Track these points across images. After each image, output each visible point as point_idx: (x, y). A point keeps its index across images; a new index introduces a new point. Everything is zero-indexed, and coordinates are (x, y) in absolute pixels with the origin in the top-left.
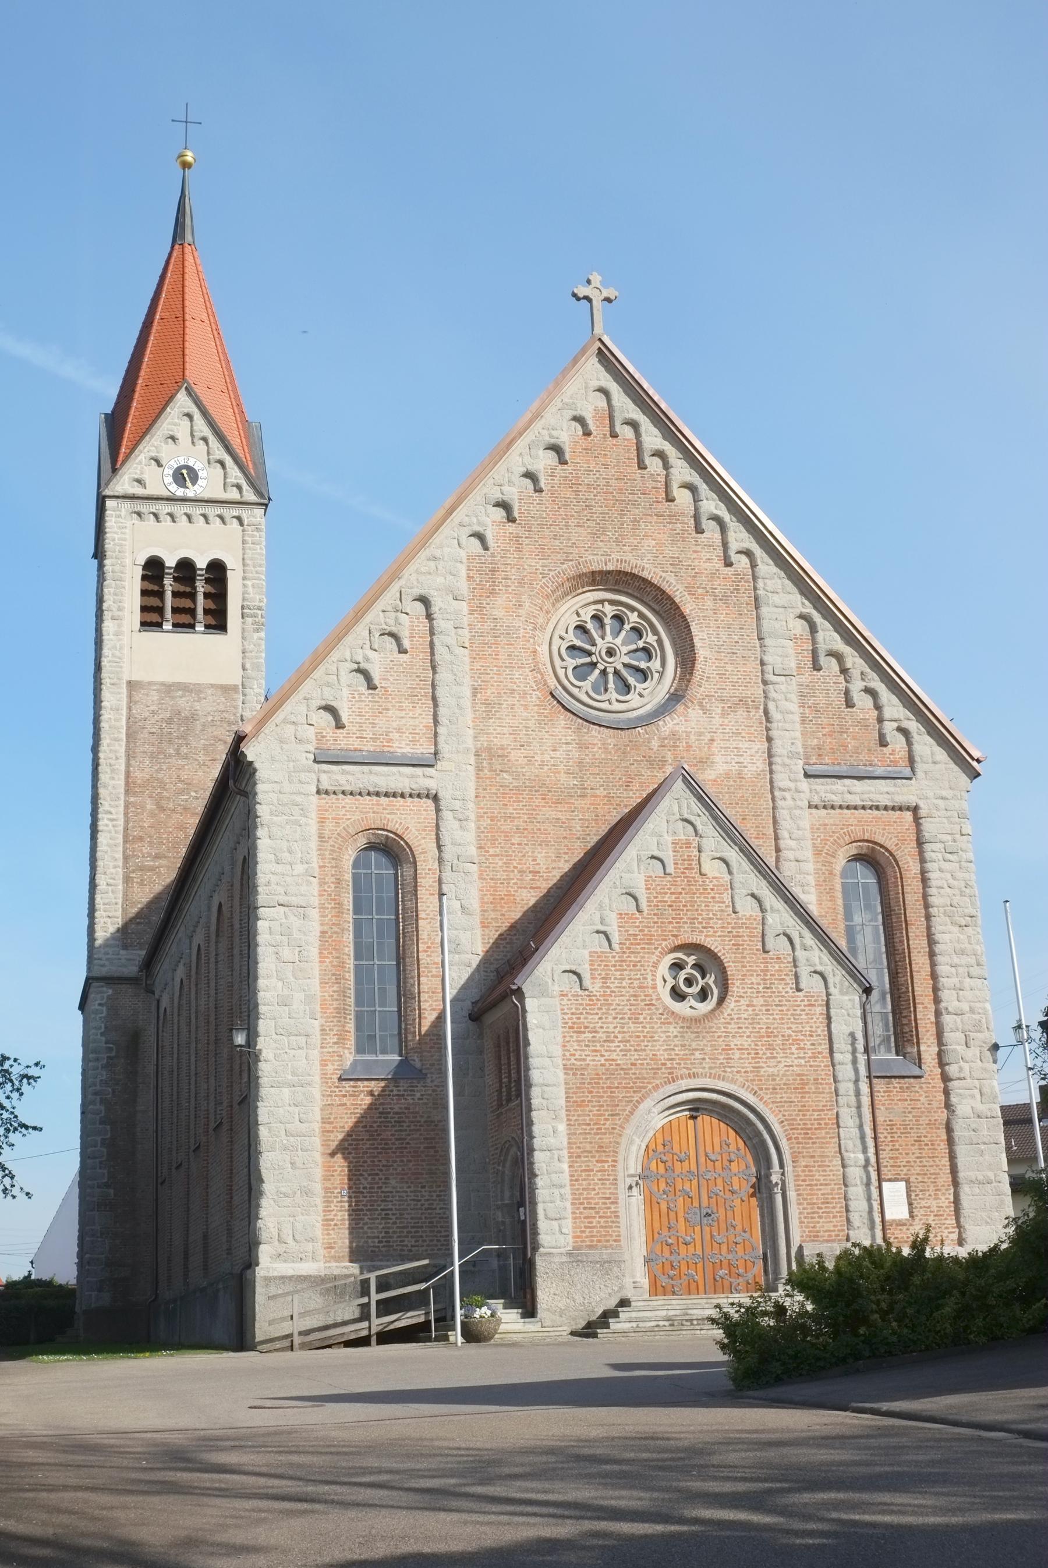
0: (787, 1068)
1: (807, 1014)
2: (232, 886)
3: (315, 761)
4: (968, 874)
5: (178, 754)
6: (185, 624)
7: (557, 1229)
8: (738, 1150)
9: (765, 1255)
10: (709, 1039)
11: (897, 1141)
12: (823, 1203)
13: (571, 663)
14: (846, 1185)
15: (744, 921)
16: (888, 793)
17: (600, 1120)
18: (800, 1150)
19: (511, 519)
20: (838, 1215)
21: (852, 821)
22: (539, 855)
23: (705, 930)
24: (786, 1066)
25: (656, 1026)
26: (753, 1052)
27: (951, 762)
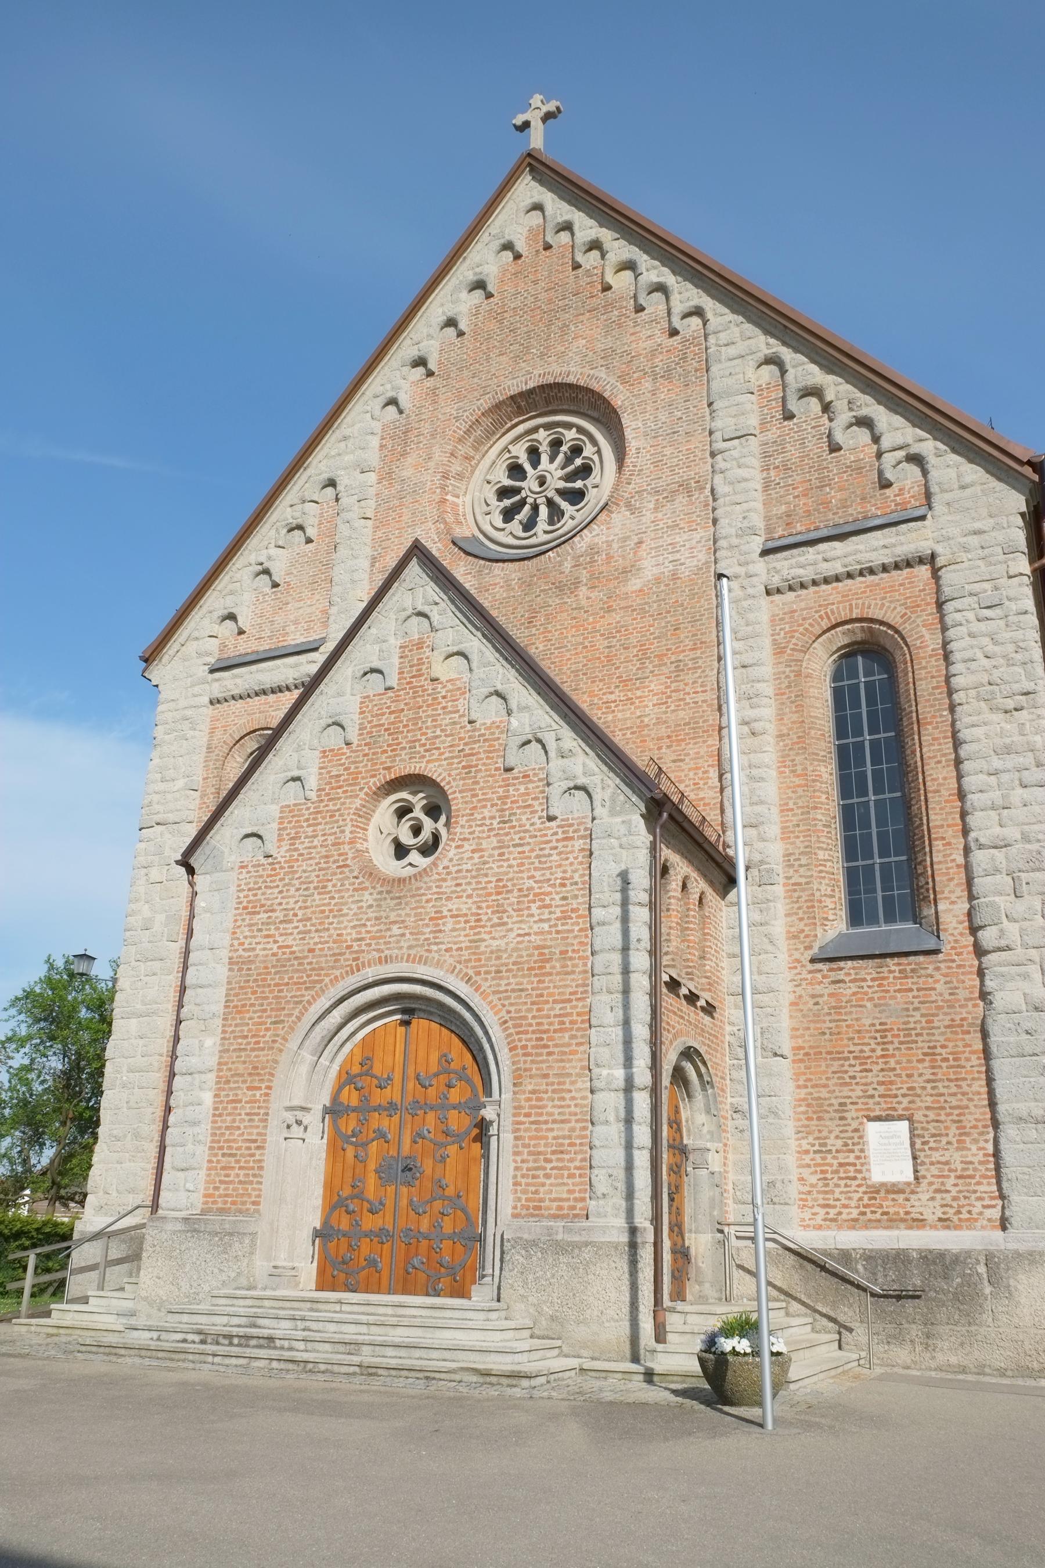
0: (519, 939)
4: (1021, 632)
10: (414, 905)
11: (893, 1056)
12: (554, 1152)
15: (483, 731)
16: (885, 547)
17: (259, 1030)
18: (528, 1066)
20: (577, 1172)
21: (835, 598)
23: (427, 754)
24: (519, 935)
25: (346, 895)
26: (473, 918)
27: (991, 479)
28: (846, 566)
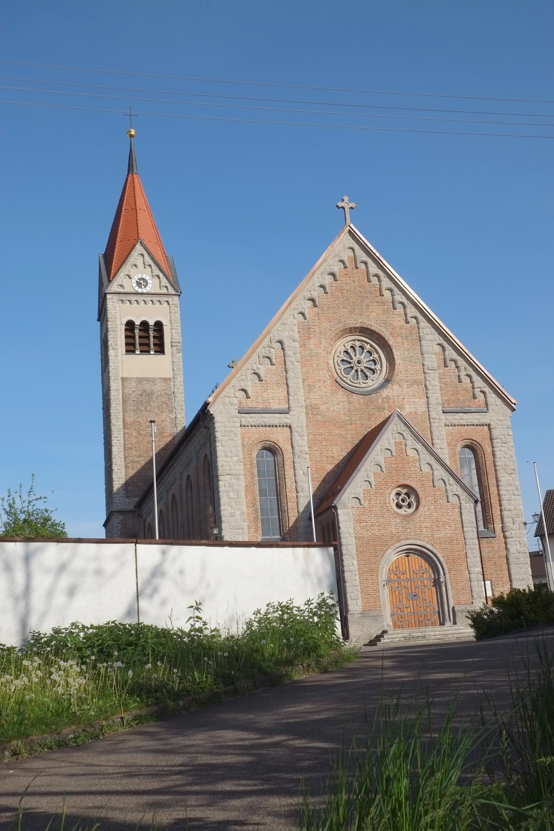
1: (452, 512)
2: (197, 467)
3: (239, 413)
5: (146, 409)
6: (145, 351)
7: (356, 603)
8: (426, 569)
9: (439, 611)
13: (343, 367)
14: (470, 581)
19: (315, 306)
21: (462, 431)
22: (334, 450)
28: (467, 422)
